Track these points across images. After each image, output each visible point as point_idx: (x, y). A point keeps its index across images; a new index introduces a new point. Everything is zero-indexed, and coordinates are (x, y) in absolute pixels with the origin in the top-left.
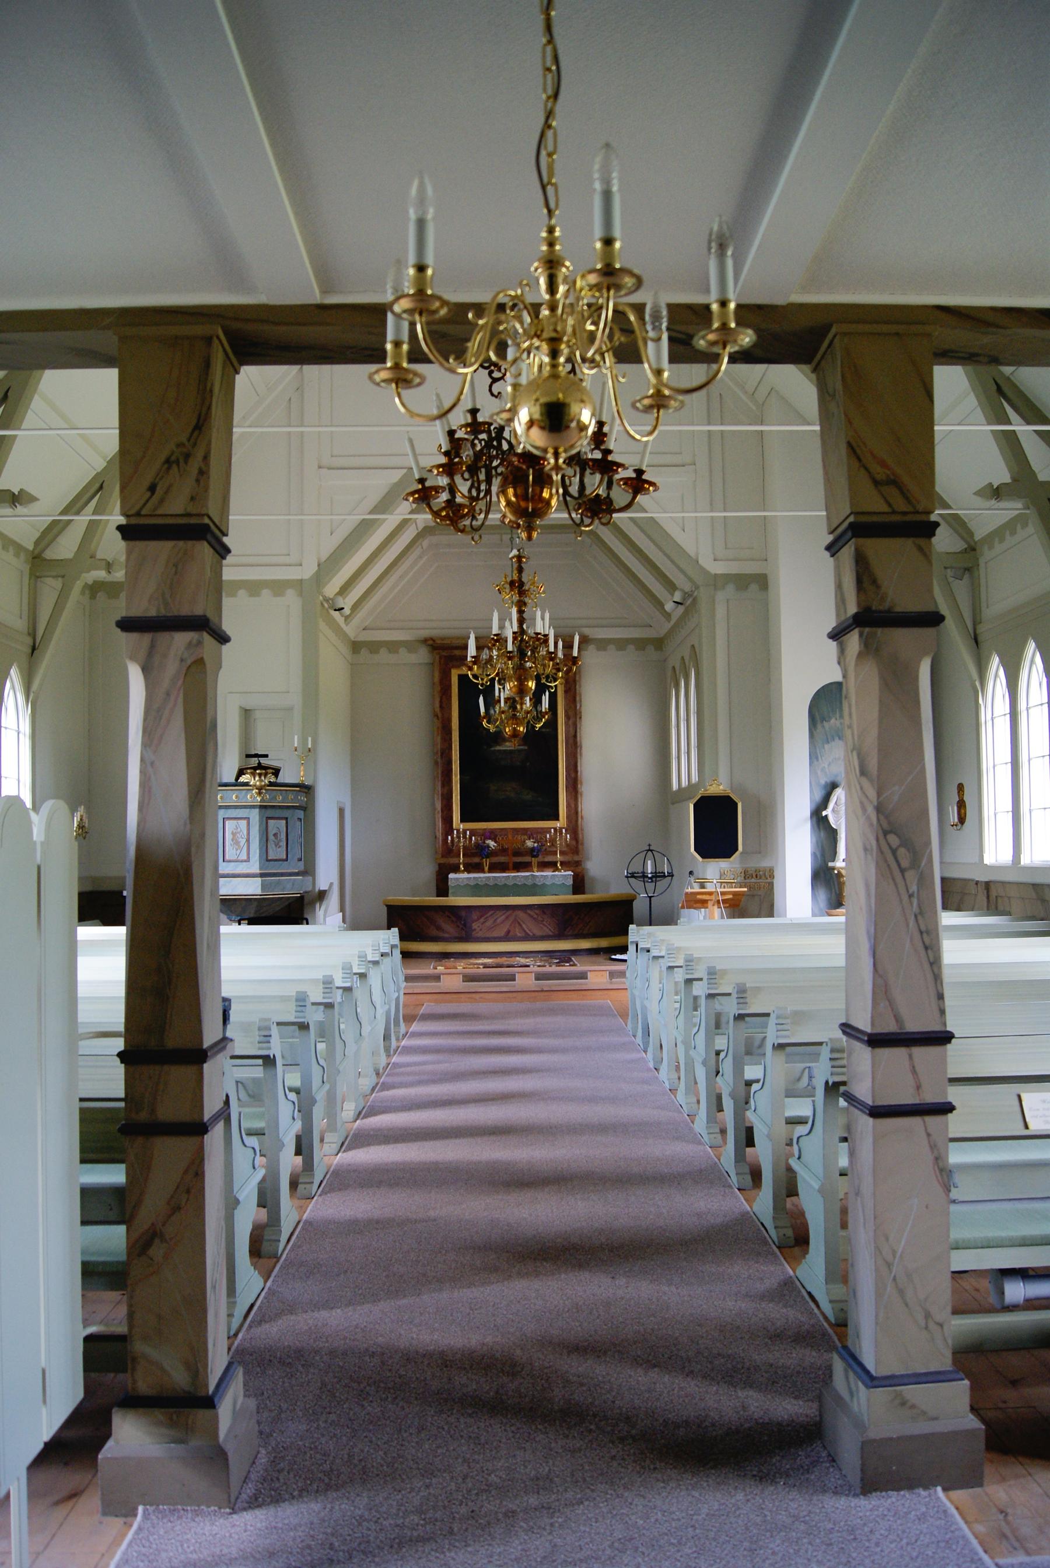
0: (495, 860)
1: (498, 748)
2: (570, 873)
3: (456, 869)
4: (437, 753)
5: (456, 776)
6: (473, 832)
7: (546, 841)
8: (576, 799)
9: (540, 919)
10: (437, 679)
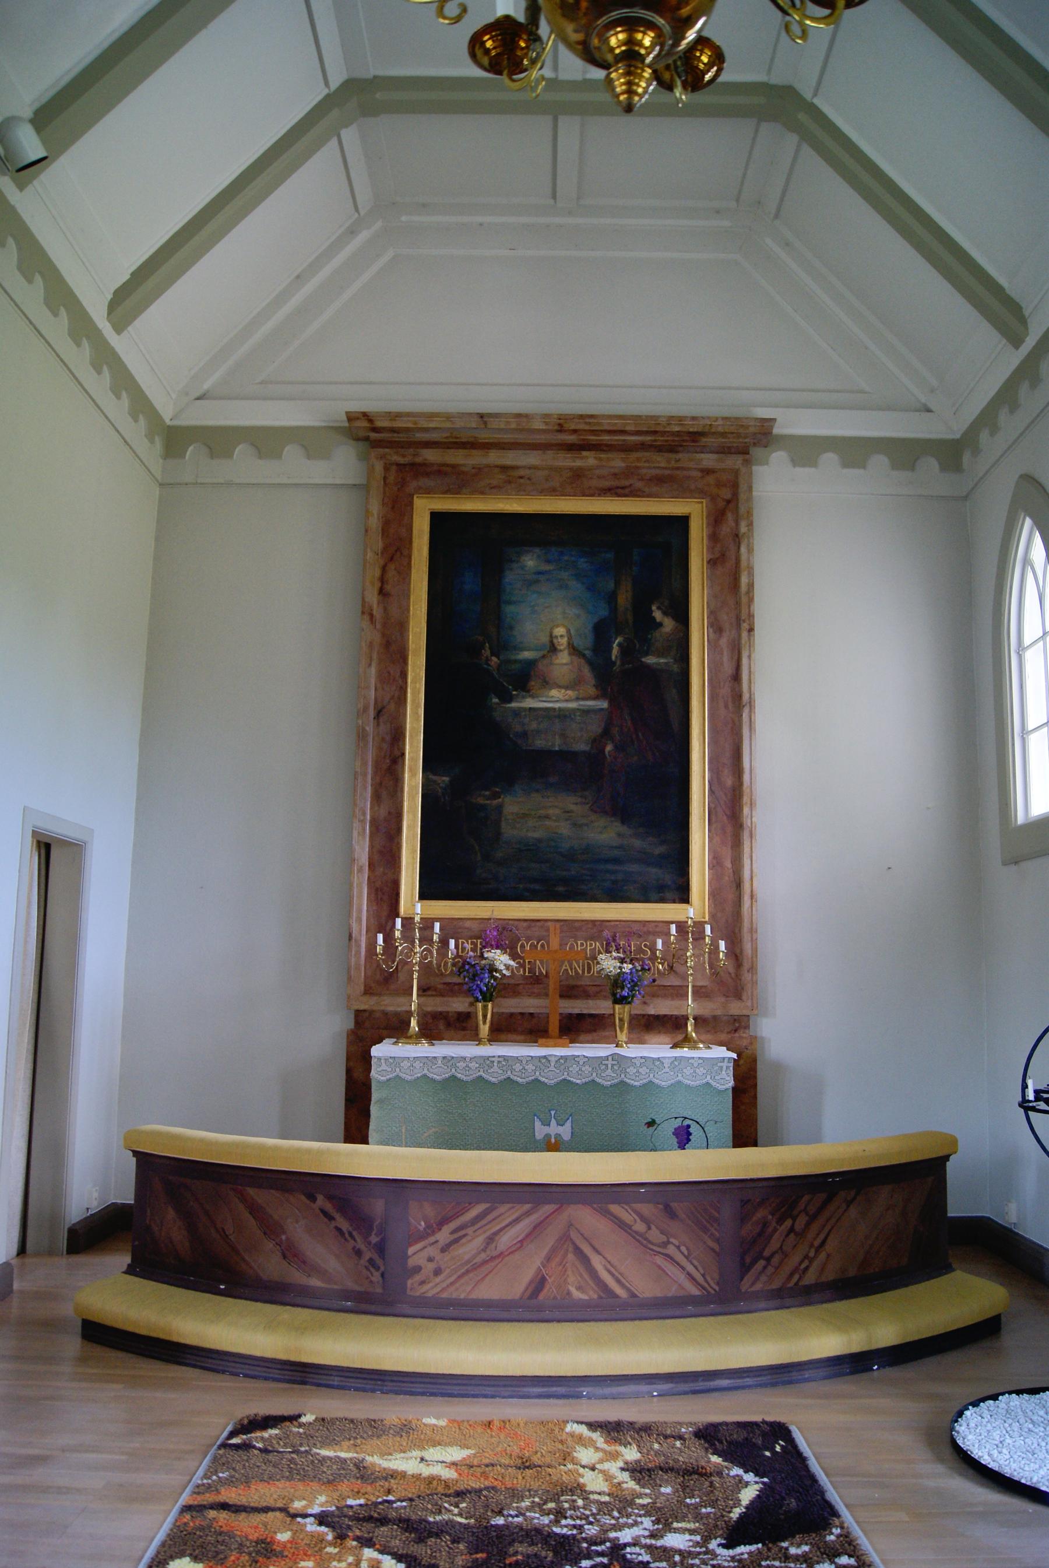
0: (512, 1005)
1: (529, 703)
2: (721, 1052)
3: (397, 1028)
4: (365, 709)
5: (413, 774)
6: (452, 928)
7: (654, 958)
8: (737, 844)
9: (655, 1235)
10: (375, 522)
